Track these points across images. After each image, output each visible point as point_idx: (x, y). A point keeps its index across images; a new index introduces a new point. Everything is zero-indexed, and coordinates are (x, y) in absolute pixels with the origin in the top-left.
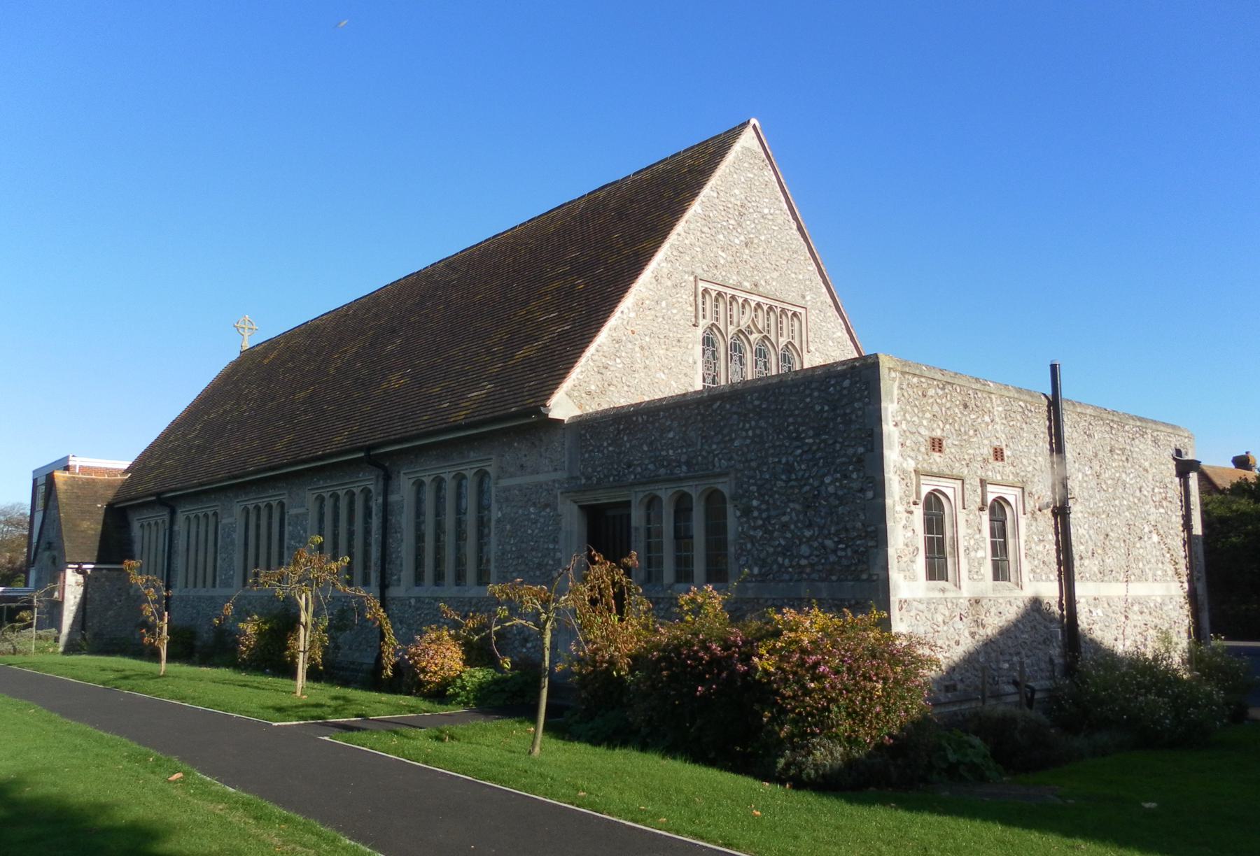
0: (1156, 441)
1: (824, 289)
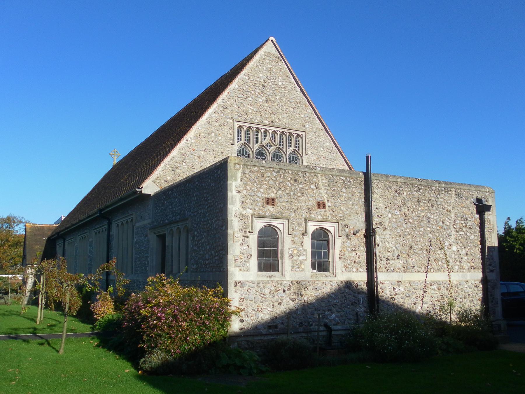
0: (458, 195)
1: (318, 121)
